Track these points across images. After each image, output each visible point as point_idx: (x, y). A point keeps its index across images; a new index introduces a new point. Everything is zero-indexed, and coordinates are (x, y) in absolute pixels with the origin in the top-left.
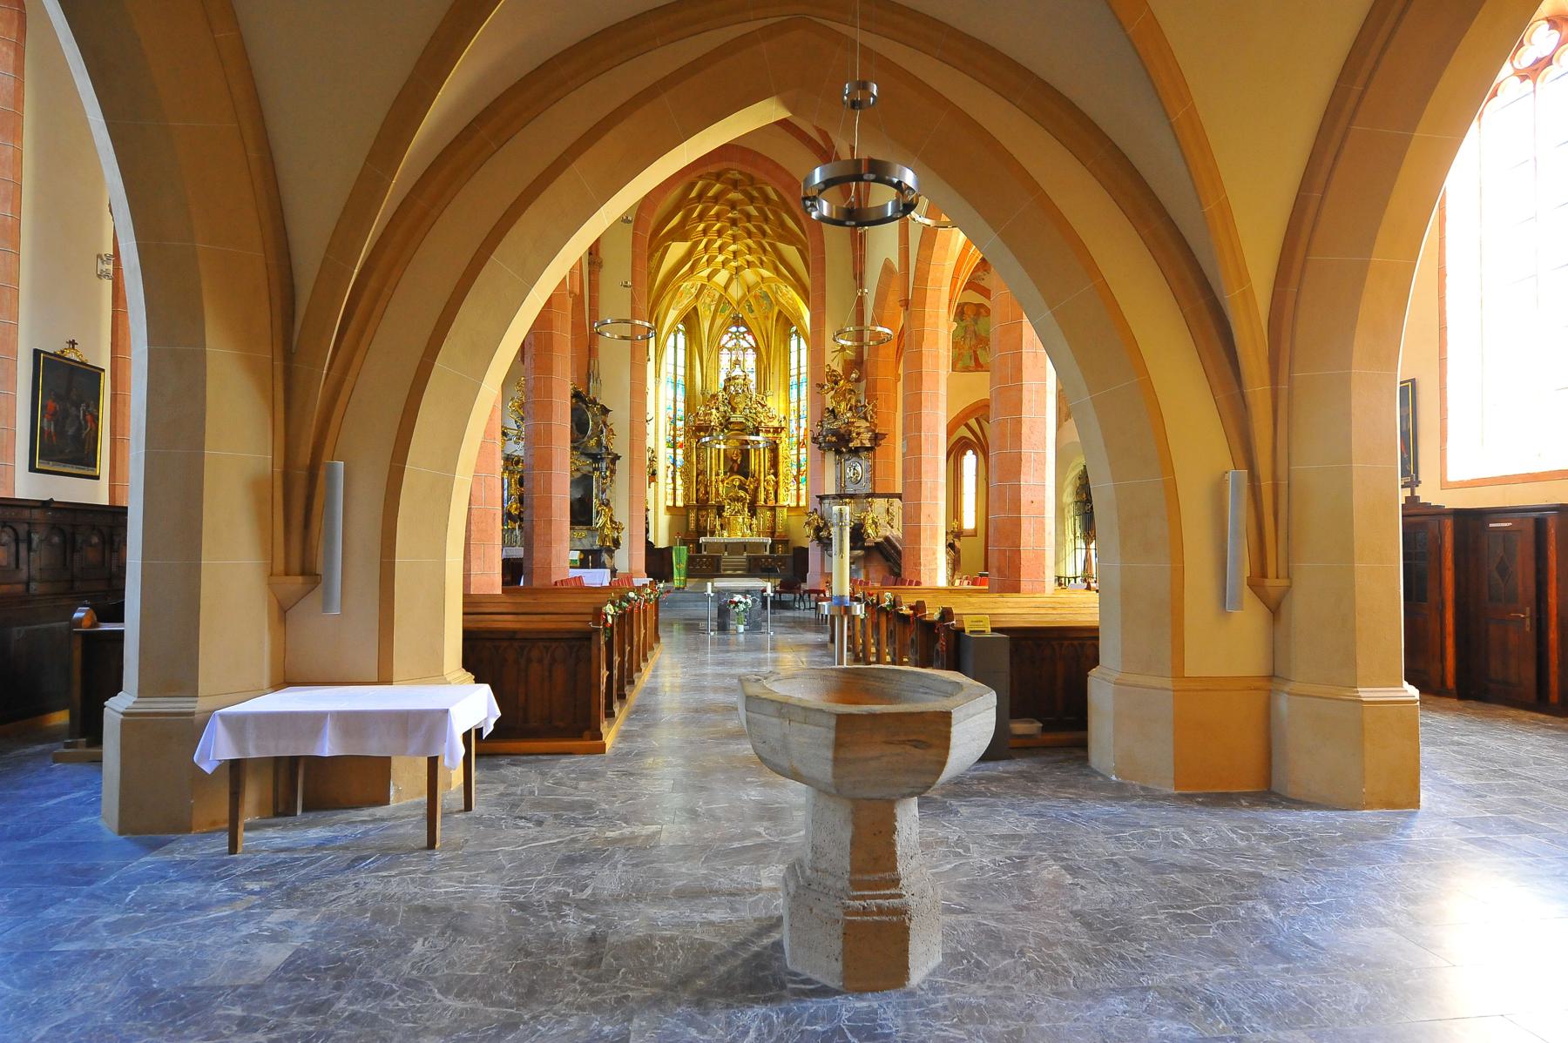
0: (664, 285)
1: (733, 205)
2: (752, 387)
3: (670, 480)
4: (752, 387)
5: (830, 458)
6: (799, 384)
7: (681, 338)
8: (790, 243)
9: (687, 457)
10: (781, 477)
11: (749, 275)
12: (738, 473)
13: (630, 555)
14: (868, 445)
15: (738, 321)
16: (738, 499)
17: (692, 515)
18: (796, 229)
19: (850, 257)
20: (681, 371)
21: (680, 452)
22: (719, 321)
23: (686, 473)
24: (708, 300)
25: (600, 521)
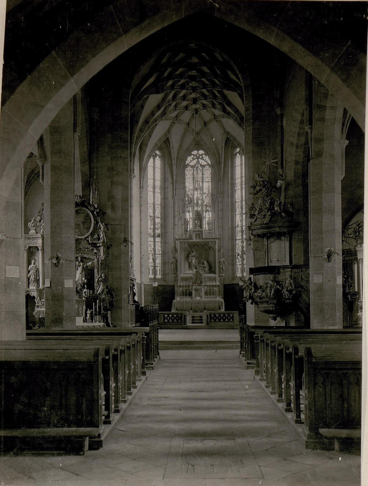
8: (233, 90)
18: (237, 80)
21: (158, 240)
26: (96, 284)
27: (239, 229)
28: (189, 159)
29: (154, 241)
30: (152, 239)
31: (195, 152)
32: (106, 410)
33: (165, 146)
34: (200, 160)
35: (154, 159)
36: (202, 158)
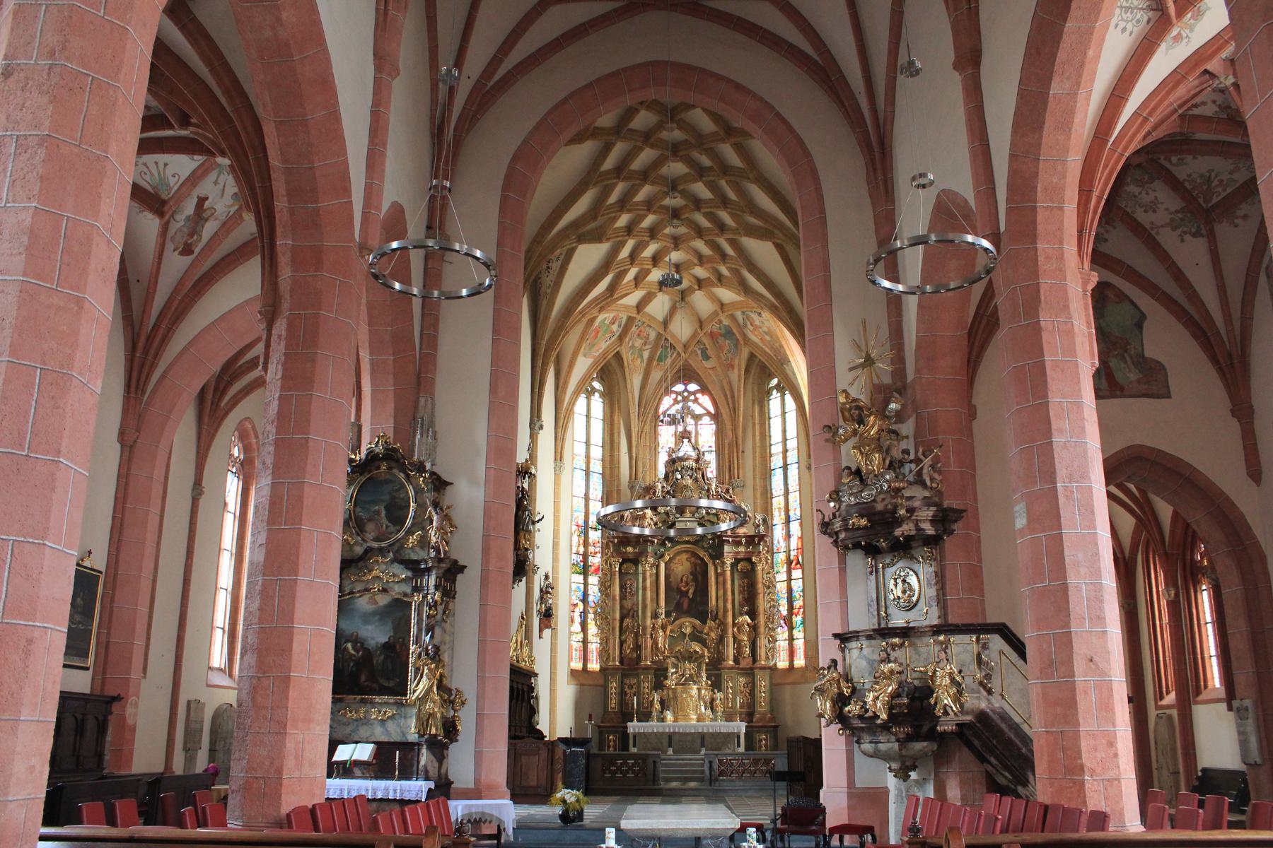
0: (568, 311)
1: (673, 185)
2: (711, 472)
3: (577, 627)
4: (711, 472)
5: (857, 561)
6: (785, 467)
7: (597, 404)
9: (605, 587)
10: (762, 619)
11: (701, 302)
12: (689, 613)
13: (478, 756)
14: (930, 530)
15: (686, 374)
16: (691, 657)
17: (613, 685)
19: (869, 216)
20: (597, 452)
21: (594, 580)
22: (656, 375)
23: (604, 618)
24: (638, 343)
25: (419, 687)
26: (411, 675)
27: (780, 558)
28: (667, 401)
29: (586, 584)
30: (582, 577)
31: (679, 387)
32: (871, 533)
33: (610, 374)
34: (690, 404)
35: (588, 398)
36: (696, 401)
